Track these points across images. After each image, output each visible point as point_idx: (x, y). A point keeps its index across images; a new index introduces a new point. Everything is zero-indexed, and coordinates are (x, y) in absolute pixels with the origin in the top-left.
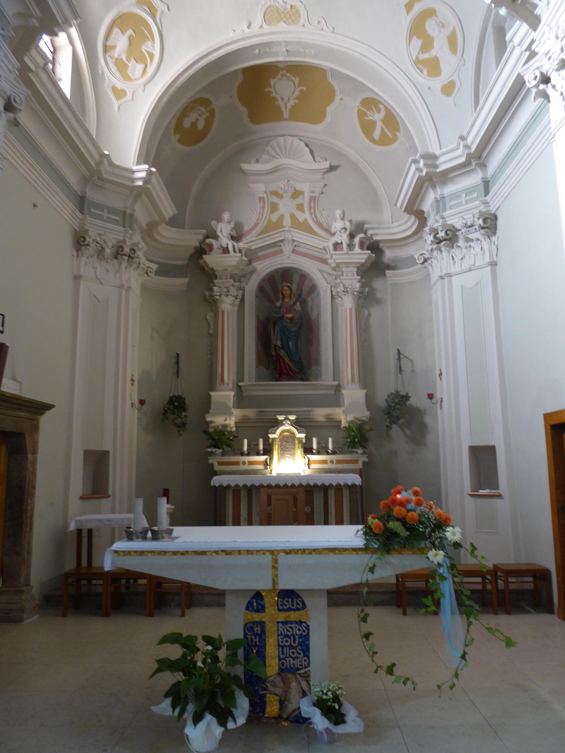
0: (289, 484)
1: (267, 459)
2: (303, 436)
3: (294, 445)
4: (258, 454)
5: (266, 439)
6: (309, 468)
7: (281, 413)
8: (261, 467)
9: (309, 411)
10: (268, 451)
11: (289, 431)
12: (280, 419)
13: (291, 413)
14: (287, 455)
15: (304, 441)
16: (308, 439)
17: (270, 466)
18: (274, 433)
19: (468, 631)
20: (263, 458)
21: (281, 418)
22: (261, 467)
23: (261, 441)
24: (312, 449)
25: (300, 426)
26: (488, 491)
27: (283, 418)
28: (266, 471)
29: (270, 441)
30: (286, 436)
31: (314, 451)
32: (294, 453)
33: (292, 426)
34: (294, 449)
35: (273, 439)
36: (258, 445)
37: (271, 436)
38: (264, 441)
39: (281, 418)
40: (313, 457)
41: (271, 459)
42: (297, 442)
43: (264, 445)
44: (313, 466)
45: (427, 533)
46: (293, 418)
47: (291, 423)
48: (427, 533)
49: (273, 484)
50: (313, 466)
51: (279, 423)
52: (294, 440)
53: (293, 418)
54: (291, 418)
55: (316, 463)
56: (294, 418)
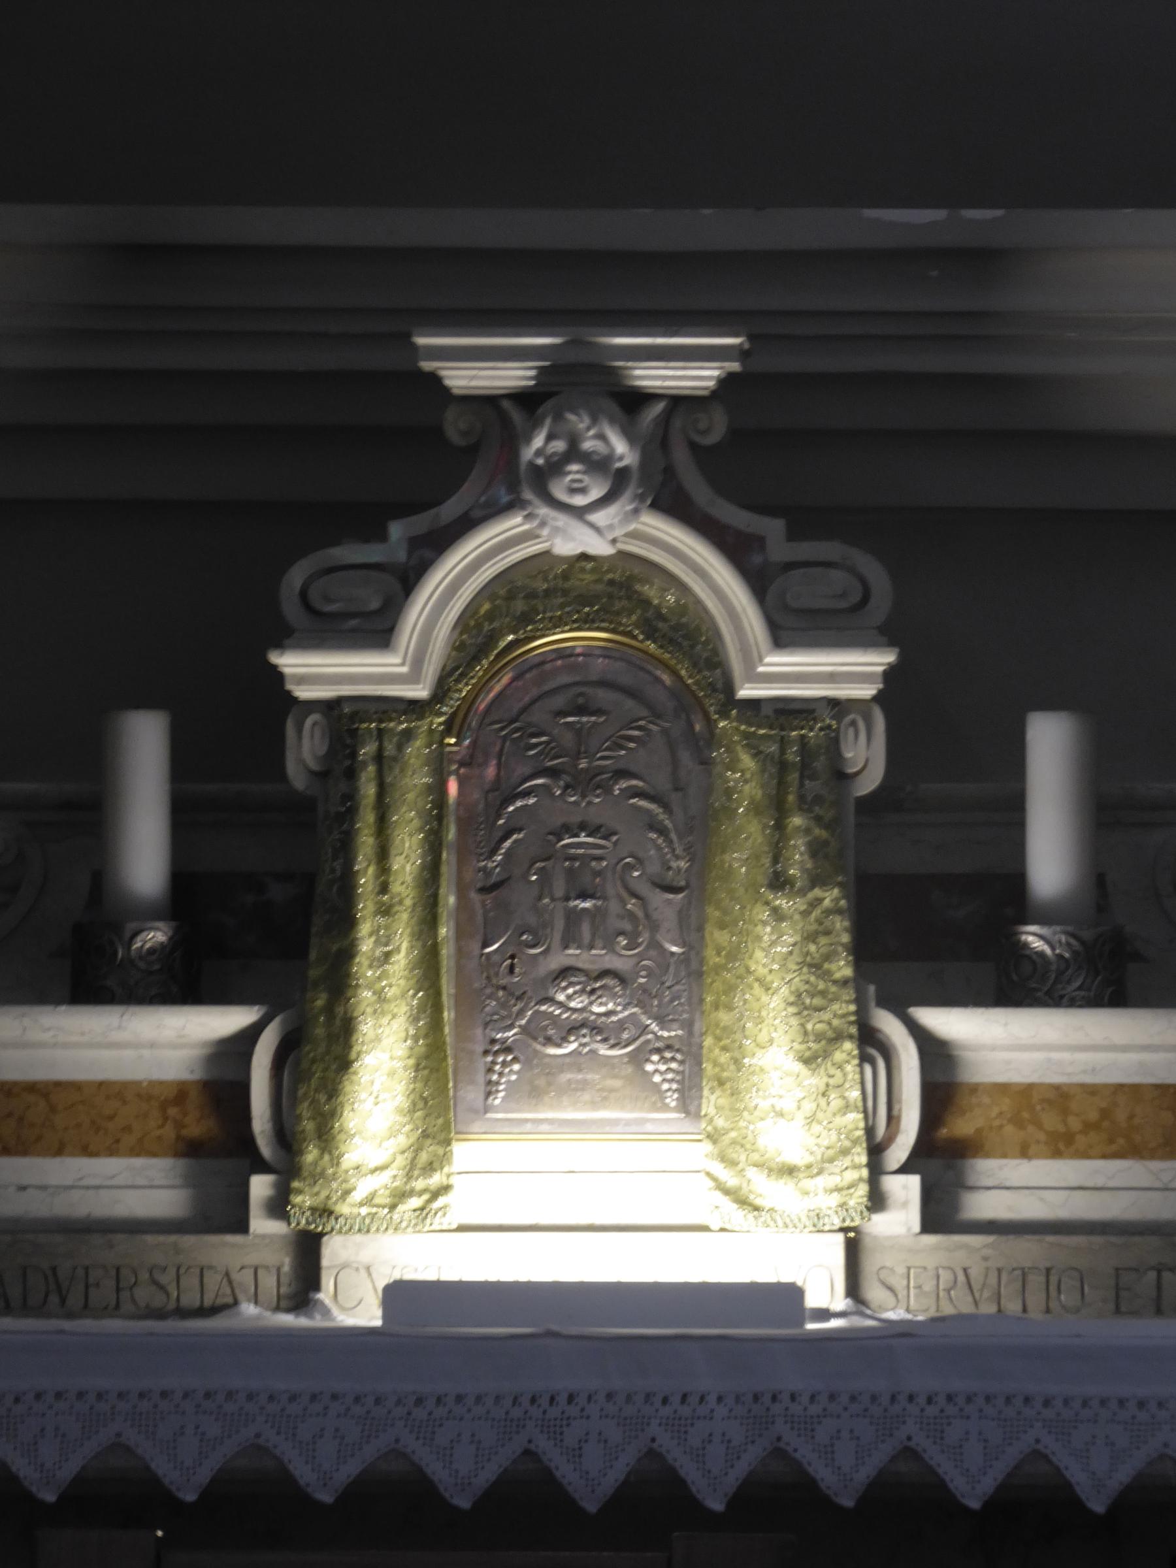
0: (592, 1473)
1: (248, 1038)
2: (852, 670)
3: (702, 830)
4: (93, 972)
5: (237, 739)
6: (938, 1215)
7: (490, 295)
8: (140, 1186)
9: (980, 261)
10: (263, 928)
11: (612, 591)
12: (462, 378)
13: (669, 295)
14: (570, 998)
15: (867, 757)
16: (949, 728)
17: (288, 1171)
18: (377, 631)
19: (756, 1209)
20: (172, 1039)
21: (482, 368)
22: (140, 1186)
23: (145, 746)
24: (1010, 895)
25: (804, 522)
26: (940, 214)
27: (513, 376)
28: (223, 1251)
29: (305, 749)
30: (577, 691)
31: (1034, 938)
32: (693, 969)
33: (672, 502)
34: (695, 889)
35: (347, 718)
36: (90, 816)
37: (315, 671)
38: (183, 764)
39: (482, 368)
40: (1000, 1041)
41: (317, 1058)
42: (744, 777)
43: (184, 815)
44: (1016, 1186)
45: (634, 618)
46: (681, 368)
47: (657, 446)
48: (634, 618)
49: (324, 1468)
50: (1016, 1186)
51: (459, 463)
52: (702, 745)
53: (681, 368)
54: (651, 376)
55: (1061, 1145)
56: (701, 377)
